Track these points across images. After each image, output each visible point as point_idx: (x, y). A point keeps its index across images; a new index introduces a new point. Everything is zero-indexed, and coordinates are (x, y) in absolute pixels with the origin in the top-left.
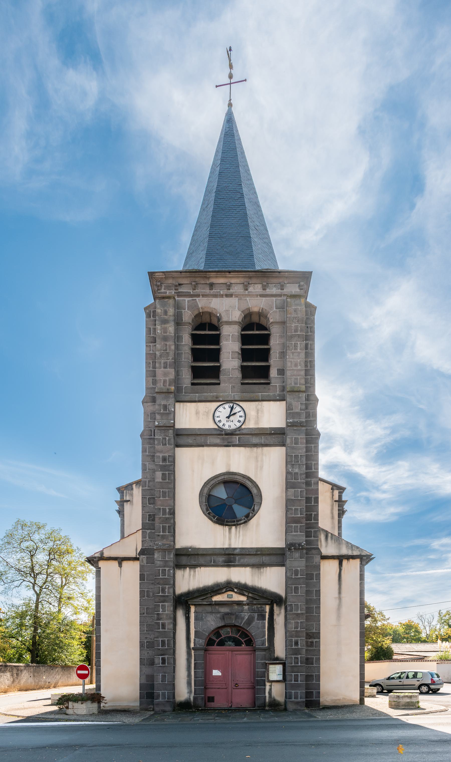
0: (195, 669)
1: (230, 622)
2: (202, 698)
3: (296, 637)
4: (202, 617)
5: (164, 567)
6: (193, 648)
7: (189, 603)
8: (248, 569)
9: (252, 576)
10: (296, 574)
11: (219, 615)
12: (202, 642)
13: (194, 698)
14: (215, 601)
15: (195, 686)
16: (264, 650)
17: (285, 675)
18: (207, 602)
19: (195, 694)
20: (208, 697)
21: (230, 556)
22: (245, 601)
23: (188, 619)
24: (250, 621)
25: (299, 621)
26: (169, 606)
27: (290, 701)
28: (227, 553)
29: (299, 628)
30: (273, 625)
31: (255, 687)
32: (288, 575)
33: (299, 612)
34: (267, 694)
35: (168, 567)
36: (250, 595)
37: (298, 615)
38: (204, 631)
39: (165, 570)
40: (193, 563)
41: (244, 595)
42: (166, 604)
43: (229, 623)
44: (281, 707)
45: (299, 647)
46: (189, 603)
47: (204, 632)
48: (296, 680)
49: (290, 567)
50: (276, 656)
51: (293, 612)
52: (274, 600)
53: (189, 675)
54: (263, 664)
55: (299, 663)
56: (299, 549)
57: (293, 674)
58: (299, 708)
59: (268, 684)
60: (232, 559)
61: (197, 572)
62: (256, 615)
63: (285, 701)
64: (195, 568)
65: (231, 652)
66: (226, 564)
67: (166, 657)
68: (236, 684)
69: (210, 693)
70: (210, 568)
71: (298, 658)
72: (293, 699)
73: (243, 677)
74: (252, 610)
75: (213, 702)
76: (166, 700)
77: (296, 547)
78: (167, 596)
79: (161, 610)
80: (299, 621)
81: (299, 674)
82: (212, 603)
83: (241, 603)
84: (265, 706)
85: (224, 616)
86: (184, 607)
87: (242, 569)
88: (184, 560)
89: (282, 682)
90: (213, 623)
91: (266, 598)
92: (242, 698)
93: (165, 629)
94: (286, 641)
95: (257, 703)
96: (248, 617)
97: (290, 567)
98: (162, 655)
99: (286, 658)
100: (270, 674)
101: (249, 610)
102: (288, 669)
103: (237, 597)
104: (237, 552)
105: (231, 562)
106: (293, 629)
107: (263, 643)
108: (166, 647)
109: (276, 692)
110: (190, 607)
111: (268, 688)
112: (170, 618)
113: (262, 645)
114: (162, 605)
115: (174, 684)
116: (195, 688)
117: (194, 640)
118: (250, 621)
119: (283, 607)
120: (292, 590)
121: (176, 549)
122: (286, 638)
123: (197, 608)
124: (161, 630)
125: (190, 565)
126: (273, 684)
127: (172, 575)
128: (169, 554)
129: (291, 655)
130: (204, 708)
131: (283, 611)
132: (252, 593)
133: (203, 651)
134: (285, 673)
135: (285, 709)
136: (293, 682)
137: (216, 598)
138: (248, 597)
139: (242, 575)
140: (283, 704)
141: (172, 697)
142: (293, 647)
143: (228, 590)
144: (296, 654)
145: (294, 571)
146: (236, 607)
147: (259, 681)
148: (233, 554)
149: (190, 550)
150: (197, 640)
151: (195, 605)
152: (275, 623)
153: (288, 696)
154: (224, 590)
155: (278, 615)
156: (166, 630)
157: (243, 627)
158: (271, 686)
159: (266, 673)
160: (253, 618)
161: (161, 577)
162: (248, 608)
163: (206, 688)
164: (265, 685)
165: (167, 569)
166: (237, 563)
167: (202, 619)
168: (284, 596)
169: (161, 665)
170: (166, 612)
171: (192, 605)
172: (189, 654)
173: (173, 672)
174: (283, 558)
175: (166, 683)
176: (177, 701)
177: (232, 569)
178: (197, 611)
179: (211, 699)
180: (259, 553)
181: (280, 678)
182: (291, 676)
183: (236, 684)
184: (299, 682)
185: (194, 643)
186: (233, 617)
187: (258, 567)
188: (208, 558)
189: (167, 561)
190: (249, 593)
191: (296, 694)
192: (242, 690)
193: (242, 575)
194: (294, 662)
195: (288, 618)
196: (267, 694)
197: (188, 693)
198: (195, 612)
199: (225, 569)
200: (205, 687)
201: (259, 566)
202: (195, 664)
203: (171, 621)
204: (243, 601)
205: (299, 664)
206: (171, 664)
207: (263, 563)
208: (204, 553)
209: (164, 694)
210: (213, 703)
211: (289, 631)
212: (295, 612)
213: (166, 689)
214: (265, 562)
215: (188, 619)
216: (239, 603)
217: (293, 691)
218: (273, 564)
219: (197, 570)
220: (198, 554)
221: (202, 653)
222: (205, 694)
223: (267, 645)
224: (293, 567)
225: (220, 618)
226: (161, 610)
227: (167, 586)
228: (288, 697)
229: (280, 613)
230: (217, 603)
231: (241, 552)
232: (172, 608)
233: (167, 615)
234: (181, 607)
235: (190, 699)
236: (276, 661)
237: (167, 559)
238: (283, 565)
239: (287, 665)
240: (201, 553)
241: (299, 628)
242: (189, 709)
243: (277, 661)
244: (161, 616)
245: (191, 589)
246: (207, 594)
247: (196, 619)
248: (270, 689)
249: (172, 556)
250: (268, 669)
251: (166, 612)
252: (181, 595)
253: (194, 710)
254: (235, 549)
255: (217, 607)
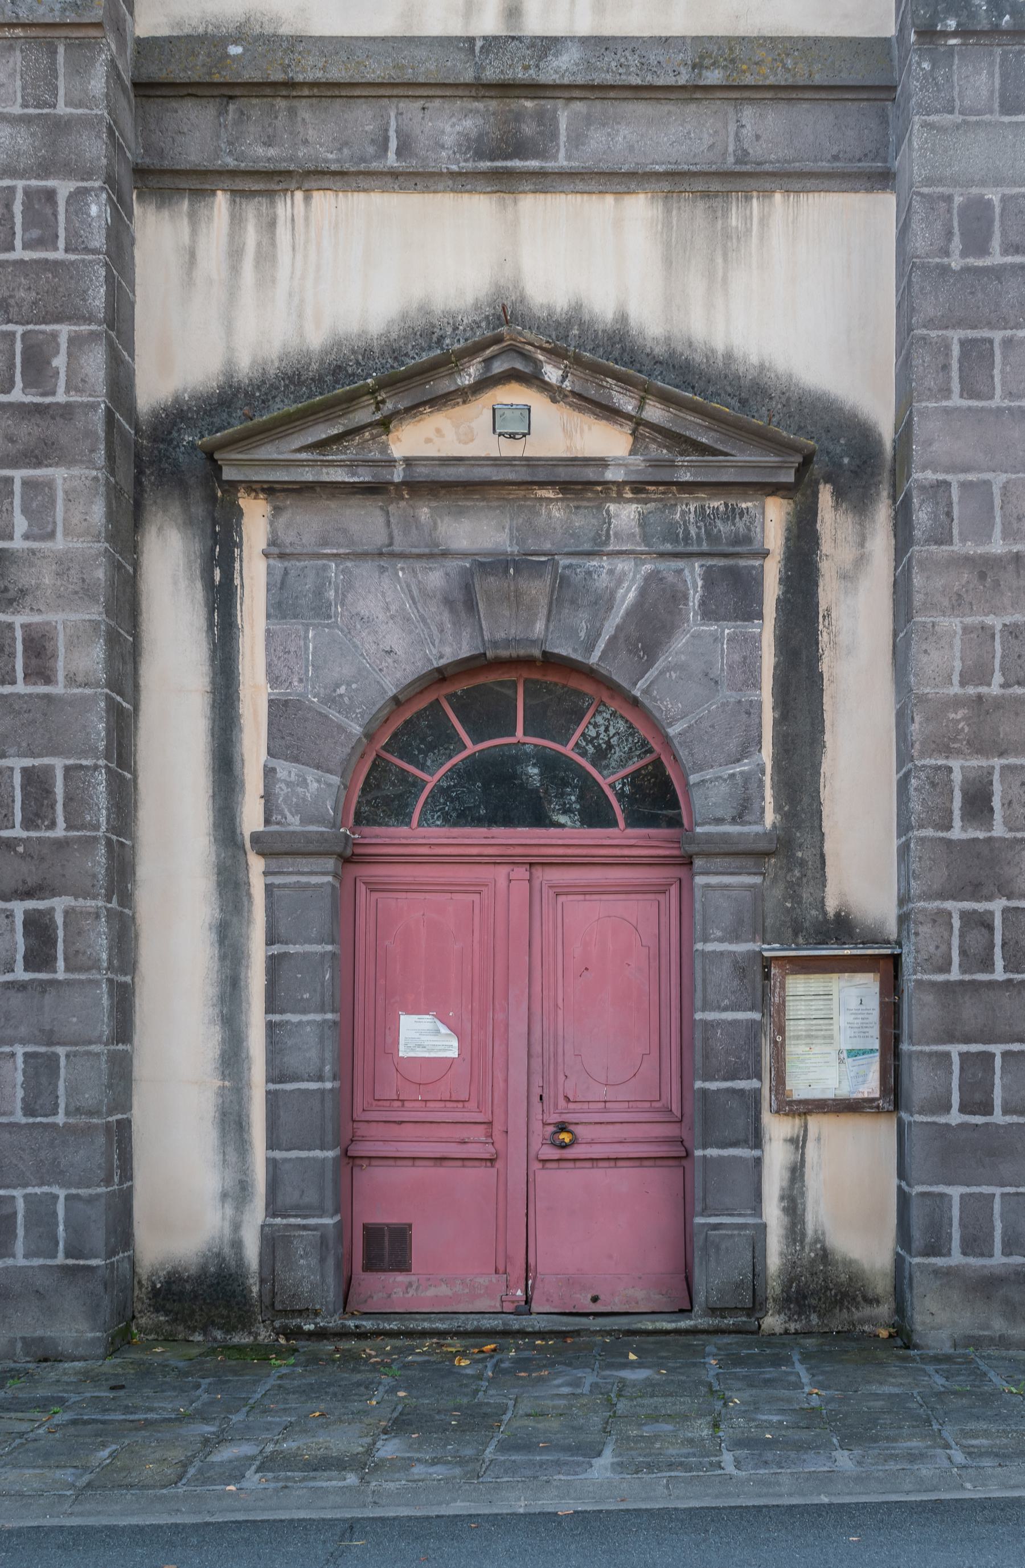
0: (272, 1005)
1: (514, 631)
2: (323, 1240)
3: (979, 747)
4: (319, 593)
5: (44, 170)
6: (256, 838)
7: (229, 474)
8: (640, 209)
9: (668, 262)
10: (977, 245)
11: (435, 578)
12: (318, 791)
13: (273, 1242)
14: (409, 462)
15: (272, 1144)
16: (753, 855)
17: (897, 1055)
18: (352, 465)
19: (273, 1208)
20: (366, 1227)
21: (515, 104)
22: (619, 463)
23: (221, 602)
24: (650, 628)
25: (995, 622)
26: (77, 491)
27: (937, 1272)
28: (490, 75)
29: (998, 678)
30: (815, 658)
31: (688, 1155)
32: (920, 243)
33: (998, 547)
34: (773, 1214)
35: (68, 171)
36: (655, 413)
37: (984, 568)
38: (331, 700)
39: (50, 195)
40: (261, 153)
41: (610, 412)
42: (58, 474)
43: (508, 643)
44: (867, 1311)
45: (999, 830)
46: (229, 474)
47: (334, 714)
48: (977, 1102)
49: (929, 181)
50: (831, 906)
51: (957, 547)
52: (822, 457)
53: (232, 1058)
54: (740, 967)
55: (999, 963)
56: (995, 31)
57: (955, 1050)
58: (999, 1325)
59: (777, 1130)
60: (529, 129)
61: (283, 233)
62: (693, 576)
63: (899, 1262)
64: (270, 194)
65: (521, 872)
66: (485, 165)
67: (59, 905)
68: (562, 1127)
69: (387, 1195)
70: (377, 199)
71: (985, 922)
72: (956, 1258)
73: (608, 1066)
74: (670, 533)
75: (402, 1265)
76: (60, 1259)
77: (973, 16)
78: (67, 411)
79: (20, 524)
80: (995, 622)
81: (997, 1049)
82: (384, 475)
83: (590, 474)
84: (756, 1307)
85: (477, 582)
86: (199, 510)
87: (599, 209)
88: (195, 133)
89: (879, 1111)
90: (395, 638)
91: (763, 439)
92: (599, 1242)
93: (48, 679)
94: (903, 784)
95: (709, 1283)
96: (643, 593)
97: (929, 181)
98: (28, 894)
99: (903, 919)
100: (794, 1050)
101: (646, 538)
102: (920, 1010)
103: (562, 433)
104: (562, 66)
105: (520, 150)
106: (956, 689)
107: (745, 809)
108: (60, 832)
109: (834, 1188)
110: (240, 513)
111: (776, 1157)
112: (87, 593)
113: (738, 818)
114: (26, 483)
115: (121, 1136)
116: (272, 1165)
117: (269, 773)
118: (650, 628)
119: (883, 513)
120: (946, 367)
121: (139, 41)
122: (903, 756)
123: (283, 520)
124: (21, 688)
125: (234, 173)
126: (816, 1124)
127: (98, 240)
128: (79, 70)
129: (942, 896)
130: (333, 1323)
131: (881, 542)
132: (666, 399)
133: (330, 863)
134: (897, 1039)
135: (902, 1336)
136: (955, 1117)
137: (422, 439)
138: (638, 425)
139: (590, 256)
140: (882, 1286)
141: (98, 1237)
142: (957, 833)
143: (499, 367)
144: (975, 890)
145: (964, 210)
146: (557, 512)
147: (709, 1111)
148: (535, 89)
149: (235, 50)
150: (286, 770)
151: (270, 490)
152: (824, 638)
153: (915, 1226)
154: (471, 373)
155: (844, 576)
156: (58, 689)
157: (605, 669)
158: (798, 1143)
159: (758, 1047)
160: (676, 597)
161: (19, 253)
162: (643, 521)
163: (350, 1160)
164: (756, 1138)
165: (64, 188)
166: (562, 161)
167: (321, 610)
168: (886, 427)
169: (20, 974)
170: (60, 543)
171: (254, 488)
172: (230, 884)
173: (105, 1029)
174: (884, 120)
175: (60, 1119)
176: (144, 1270)
177: (531, 205)
178: (288, 538)
179: (388, 1248)
180: (713, 77)
181: (870, 1086)
182: (938, 1065)
183: (562, 1127)
184: (998, 1117)
185: (268, 797)
186: (537, 589)
187: (706, 195)
188: (362, 118)
189: (60, 126)
190: (646, 392)
191: (977, 1209)
192: (600, 1175)
193: (590, 256)
194: (963, 953)
195: (918, 599)
196: (773, 1214)
197: (224, 1196)
198: (277, 551)
199: (479, 208)
200: (345, 1152)
201: (715, 186)
202: (274, 964)
203: (95, 613)
204: (602, 463)
205: (999, 974)
206: (95, 965)
207: (742, 157)
208: (336, 74)
209: (41, 1213)
210: (401, 1278)
211: (922, 699)
212: (971, 548)
213: (53, 1173)
214: (756, 151)
215: (221, 602)
216: (578, 482)
217: (955, 1192)
218: (810, 166)
219: (283, 209)
220: (290, 85)
221: (318, 875)
222: (344, 1201)
223: (770, 817)
224: (955, 182)
225: (448, 602)
226: (20, 524)
227: (64, 330)
228: (916, 1233)
229: (861, 560)
230: (422, 473)
231: (589, 66)
232: (98, 512)
233: (63, 564)
234: (176, 509)
235: (237, 1245)
236: (834, 942)
237: (62, 109)
238: (882, 179)
239: (911, 976)
240: (311, 76)
241: (998, 678)
242: (229, 1330)
243: (841, 943)
244: (24, 578)
245: (245, 365)
246: (351, 400)
247: (281, 606)
248: (796, 1172)
249: (98, 84)
250: (782, 1007)
251: (60, 543)
252: (176, 416)
253: (265, 1335)
254: (547, 46)
255: (424, 513)
